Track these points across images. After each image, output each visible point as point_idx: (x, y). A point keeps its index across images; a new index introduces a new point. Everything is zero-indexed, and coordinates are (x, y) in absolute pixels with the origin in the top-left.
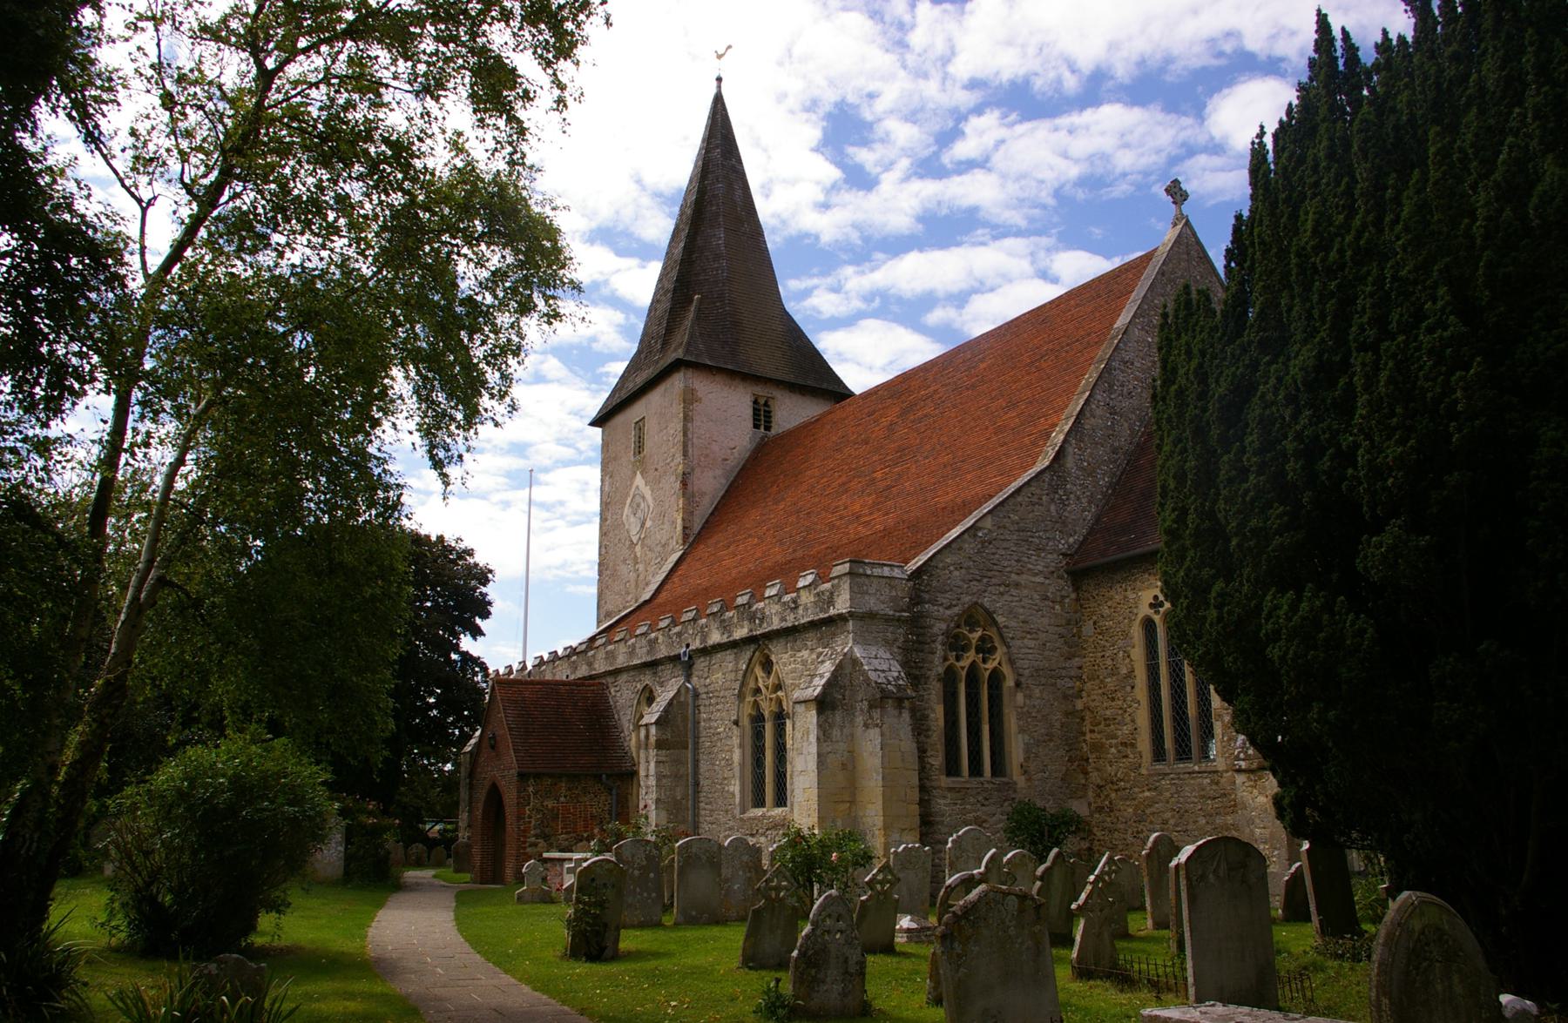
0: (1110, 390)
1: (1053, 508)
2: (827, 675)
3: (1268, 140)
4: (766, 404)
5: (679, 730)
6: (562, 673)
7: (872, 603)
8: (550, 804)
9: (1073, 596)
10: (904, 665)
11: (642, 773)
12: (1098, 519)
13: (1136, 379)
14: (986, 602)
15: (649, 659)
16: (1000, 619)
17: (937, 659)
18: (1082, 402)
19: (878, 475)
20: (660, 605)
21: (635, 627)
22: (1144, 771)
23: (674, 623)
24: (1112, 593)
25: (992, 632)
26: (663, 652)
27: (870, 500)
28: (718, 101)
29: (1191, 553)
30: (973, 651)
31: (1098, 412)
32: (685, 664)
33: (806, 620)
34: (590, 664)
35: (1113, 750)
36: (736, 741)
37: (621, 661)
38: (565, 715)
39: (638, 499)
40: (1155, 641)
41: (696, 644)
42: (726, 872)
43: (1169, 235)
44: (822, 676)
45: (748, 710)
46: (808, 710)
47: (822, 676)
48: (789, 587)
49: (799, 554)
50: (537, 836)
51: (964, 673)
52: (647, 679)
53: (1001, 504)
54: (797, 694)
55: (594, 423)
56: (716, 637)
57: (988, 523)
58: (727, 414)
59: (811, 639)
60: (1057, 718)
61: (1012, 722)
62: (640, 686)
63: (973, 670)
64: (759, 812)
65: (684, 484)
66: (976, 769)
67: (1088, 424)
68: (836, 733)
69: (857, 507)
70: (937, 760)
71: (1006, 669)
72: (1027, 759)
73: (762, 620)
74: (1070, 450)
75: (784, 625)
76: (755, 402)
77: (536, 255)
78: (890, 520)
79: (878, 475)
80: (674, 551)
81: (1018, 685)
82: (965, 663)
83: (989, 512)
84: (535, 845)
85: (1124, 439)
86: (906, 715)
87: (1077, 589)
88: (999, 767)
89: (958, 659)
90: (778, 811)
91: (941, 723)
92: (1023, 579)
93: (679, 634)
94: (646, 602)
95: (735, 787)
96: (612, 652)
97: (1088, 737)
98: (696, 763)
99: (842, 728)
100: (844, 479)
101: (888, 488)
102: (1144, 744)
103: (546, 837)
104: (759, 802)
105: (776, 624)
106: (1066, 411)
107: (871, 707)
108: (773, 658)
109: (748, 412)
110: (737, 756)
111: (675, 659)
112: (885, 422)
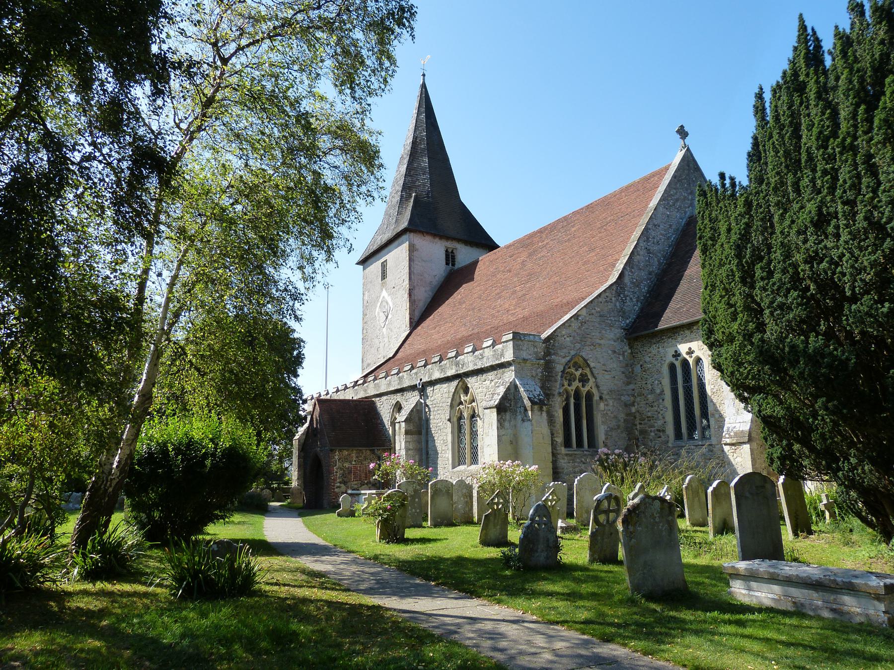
0: (648, 240)
1: (618, 304)
2: (501, 394)
3: (768, 96)
4: (452, 252)
5: (419, 424)
6: (349, 395)
7: (525, 355)
8: (347, 465)
9: (629, 351)
10: (541, 388)
11: (397, 448)
12: (642, 310)
13: (661, 234)
14: (583, 354)
16: (592, 365)
17: (558, 385)
18: (632, 247)
19: (518, 288)
20: (399, 360)
21: (391, 370)
22: (670, 445)
23: (412, 368)
24: (651, 349)
25: (587, 371)
26: (406, 384)
28: (424, 86)
29: (741, 315)
31: (641, 253)
32: (422, 389)
33: (488, 365)
34: (365, 391)
35: (653, 434)
36: (450, 430)
39: (384, 304)
40: (676, 375)
42: (455, 498)
43: (679, 155)
47: (498, 395)
49: (476, 331)
50: (340, 483)
51: (573, 393)
52: (398, 397)
53: (591, 302)
54: (484, 404)
56: (437, 375)
57: (584, 312)
58: (434, 250)
59: (491, 375)
60: (622, 416)
61: (598, 419)
62: (394, 402)
63: (577, 394)
64: (462, 467)
65: (410, 295)
66: (580, 444)
67: (636, 258)
68: (507, 424)
69: (507, 306)
70: (560, 439)
71: (595, 391)
72: (606, 439)
73: (463, 365)
74: (626, 273)
75: (476, 368)
76: (447, 251)
77: (367, 155)
78: (526, 313)
79: (518, 288)
81: (601, 398)
82: (573, 387)
83: (585, 306)
85: (654, 268)
86: (544, 414)
87: (631, 348)
88: (592, 444)
91: (562, 419)
92: (602, 342)
93: (416, 374)
94: (390, 359)
97: (638, 427)
99: (510, 421)
100: (498, 291)
101: (524, 295)
102: (670, 430)
103: (345, 483)
105: (471, 367)
106: (624, 252)
111: (413, 388)
112: (519, 260)
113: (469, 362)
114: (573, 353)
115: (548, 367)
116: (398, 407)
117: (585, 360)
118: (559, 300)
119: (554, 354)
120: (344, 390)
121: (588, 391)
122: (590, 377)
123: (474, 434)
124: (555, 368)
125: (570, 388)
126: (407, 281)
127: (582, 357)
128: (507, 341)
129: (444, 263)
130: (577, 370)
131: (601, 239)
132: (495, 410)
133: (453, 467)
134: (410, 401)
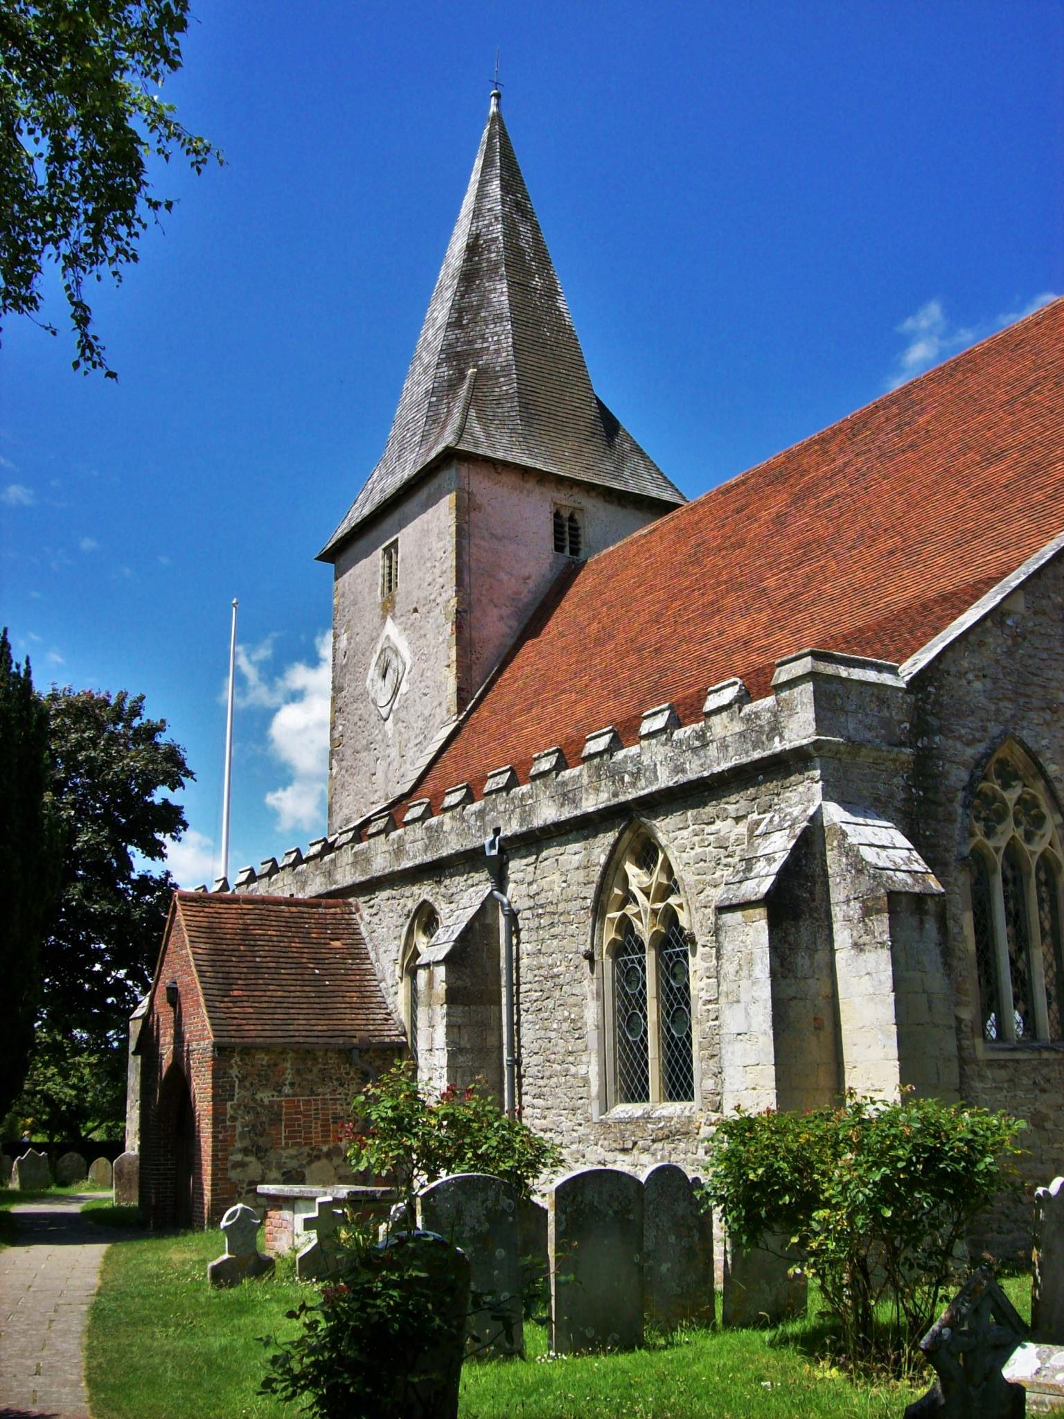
2: (781, 858)
4: (572, 519)
5: (477, 975)
8: (265, 1096)
15: (428, 858)
16: (1052, 769)
19: (771, 582)
26: (452, 846)
27: (764, 618)
30: (1010, 820)
32: (492, 863)
34: (329, 874)
37: (381, 864)
38: (288, 947)
41: (512, 828)
44: (769, 859)
45: (610, 934)
46: (748, 922)
48: (687, 710)
50: (245, 1151)
51: (999, 859)
52: (423, 891)
55: (319, 558)
56: (548, 813)
62: (412, 905)
63: (1012, 854)
64: (636, 1109)
75: (681, 778)
76: (557, 515)
80: (444, 724)
83: (1021, 586)
84: (242, 1165)
86: (931, 925)
89: (989, 833)
90: (674, 1109)
91: (971, 946)
93: (481, 814)
95: (590, 1067)
96: (363, 852)
98: (515, 1027)
101: (792, 596)
103: (258, 1151)
104: (636, 1092)
105: (665, 779)
107: (867, 912)
108: (662, 838)
109: (547, 528)
110: (591, 1013)
113: (657, 763)
114: (995, 729)
115: (924, 770)
116: (426, 919)
117: (1032, 755)
118: (908, 595)
119: (940, 731)
120: (269, 874)
121: (1043, 856)
122: (1045, 809)
123: (677, 1002)
124: (945, 775)
125: (991, 844)
126: (451, 591)
127: (1022, 743)
128: (792, 683)
129: (550, 545)
130: (1006, 786)
131: (1015, 427)
132: (761, 912)
133: (605, 1108)
134: (461, 901)
